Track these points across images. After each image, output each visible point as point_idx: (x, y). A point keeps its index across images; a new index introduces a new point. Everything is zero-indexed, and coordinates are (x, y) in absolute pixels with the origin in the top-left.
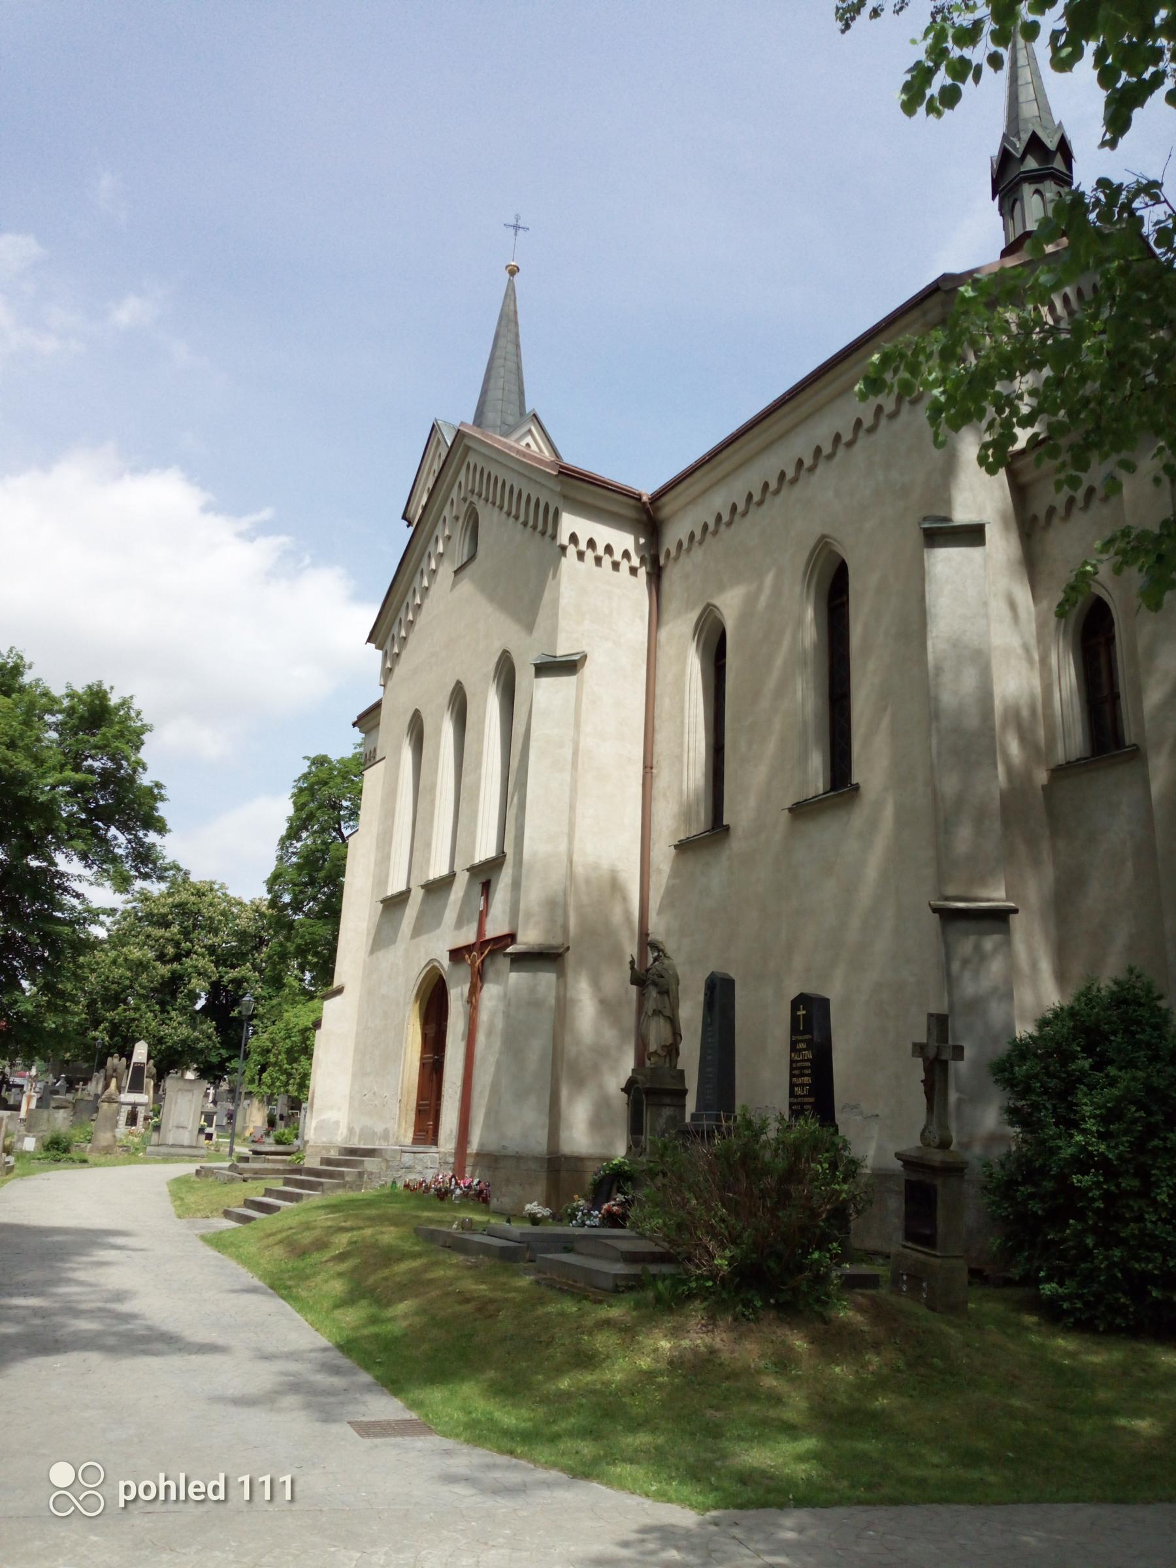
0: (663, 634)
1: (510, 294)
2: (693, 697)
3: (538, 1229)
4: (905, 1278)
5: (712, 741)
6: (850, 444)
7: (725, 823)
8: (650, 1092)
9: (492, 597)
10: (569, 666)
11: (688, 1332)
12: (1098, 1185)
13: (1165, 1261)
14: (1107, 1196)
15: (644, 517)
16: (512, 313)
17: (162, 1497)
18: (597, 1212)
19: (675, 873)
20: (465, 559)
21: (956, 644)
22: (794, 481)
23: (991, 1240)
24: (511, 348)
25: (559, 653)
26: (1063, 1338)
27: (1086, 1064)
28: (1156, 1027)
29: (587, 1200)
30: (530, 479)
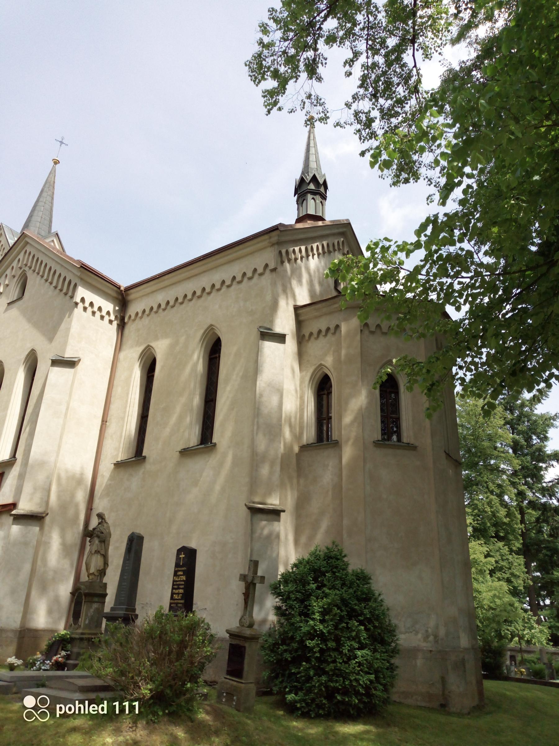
0: (122, 355)
1: (53, 173)
2: (134, 389)
3: (16, 673)
4: (225, 694)
5: (141, 412)
6: (229, 286)
7: (144, 454)
8: (87, 595)
9: (29, 320)
10: (71, 364)
11: (122, 732)
12: (318, 645)
13: (344, 681)
14: (322, 651)
15: (120, 297)
16: (52, 182)
17: (77, 712)
18: (49, 662)
19: (112, 478)
20: (15, 299)
21: (269, 385)
22: (199, 297)
23: (264, 673)
24: (49, 198)
25: (66, 356)
26: (296, 722)
27: (314, 586)
28: (344, 570)
29: (42, 655)
30: (62, 266)
